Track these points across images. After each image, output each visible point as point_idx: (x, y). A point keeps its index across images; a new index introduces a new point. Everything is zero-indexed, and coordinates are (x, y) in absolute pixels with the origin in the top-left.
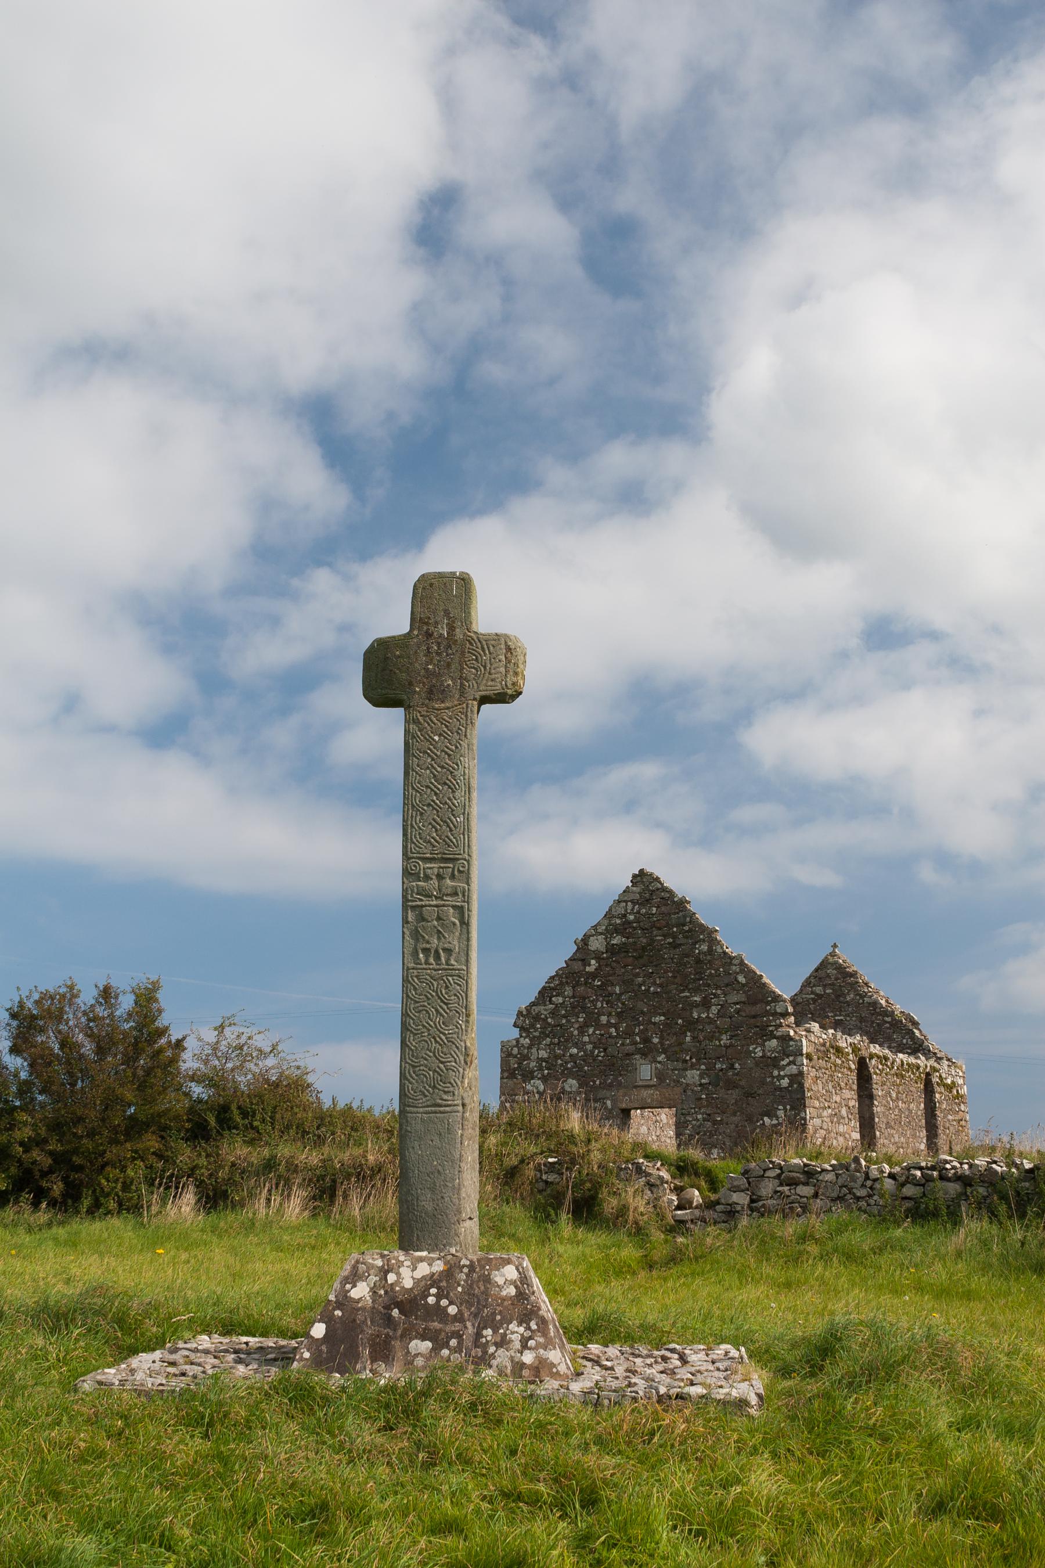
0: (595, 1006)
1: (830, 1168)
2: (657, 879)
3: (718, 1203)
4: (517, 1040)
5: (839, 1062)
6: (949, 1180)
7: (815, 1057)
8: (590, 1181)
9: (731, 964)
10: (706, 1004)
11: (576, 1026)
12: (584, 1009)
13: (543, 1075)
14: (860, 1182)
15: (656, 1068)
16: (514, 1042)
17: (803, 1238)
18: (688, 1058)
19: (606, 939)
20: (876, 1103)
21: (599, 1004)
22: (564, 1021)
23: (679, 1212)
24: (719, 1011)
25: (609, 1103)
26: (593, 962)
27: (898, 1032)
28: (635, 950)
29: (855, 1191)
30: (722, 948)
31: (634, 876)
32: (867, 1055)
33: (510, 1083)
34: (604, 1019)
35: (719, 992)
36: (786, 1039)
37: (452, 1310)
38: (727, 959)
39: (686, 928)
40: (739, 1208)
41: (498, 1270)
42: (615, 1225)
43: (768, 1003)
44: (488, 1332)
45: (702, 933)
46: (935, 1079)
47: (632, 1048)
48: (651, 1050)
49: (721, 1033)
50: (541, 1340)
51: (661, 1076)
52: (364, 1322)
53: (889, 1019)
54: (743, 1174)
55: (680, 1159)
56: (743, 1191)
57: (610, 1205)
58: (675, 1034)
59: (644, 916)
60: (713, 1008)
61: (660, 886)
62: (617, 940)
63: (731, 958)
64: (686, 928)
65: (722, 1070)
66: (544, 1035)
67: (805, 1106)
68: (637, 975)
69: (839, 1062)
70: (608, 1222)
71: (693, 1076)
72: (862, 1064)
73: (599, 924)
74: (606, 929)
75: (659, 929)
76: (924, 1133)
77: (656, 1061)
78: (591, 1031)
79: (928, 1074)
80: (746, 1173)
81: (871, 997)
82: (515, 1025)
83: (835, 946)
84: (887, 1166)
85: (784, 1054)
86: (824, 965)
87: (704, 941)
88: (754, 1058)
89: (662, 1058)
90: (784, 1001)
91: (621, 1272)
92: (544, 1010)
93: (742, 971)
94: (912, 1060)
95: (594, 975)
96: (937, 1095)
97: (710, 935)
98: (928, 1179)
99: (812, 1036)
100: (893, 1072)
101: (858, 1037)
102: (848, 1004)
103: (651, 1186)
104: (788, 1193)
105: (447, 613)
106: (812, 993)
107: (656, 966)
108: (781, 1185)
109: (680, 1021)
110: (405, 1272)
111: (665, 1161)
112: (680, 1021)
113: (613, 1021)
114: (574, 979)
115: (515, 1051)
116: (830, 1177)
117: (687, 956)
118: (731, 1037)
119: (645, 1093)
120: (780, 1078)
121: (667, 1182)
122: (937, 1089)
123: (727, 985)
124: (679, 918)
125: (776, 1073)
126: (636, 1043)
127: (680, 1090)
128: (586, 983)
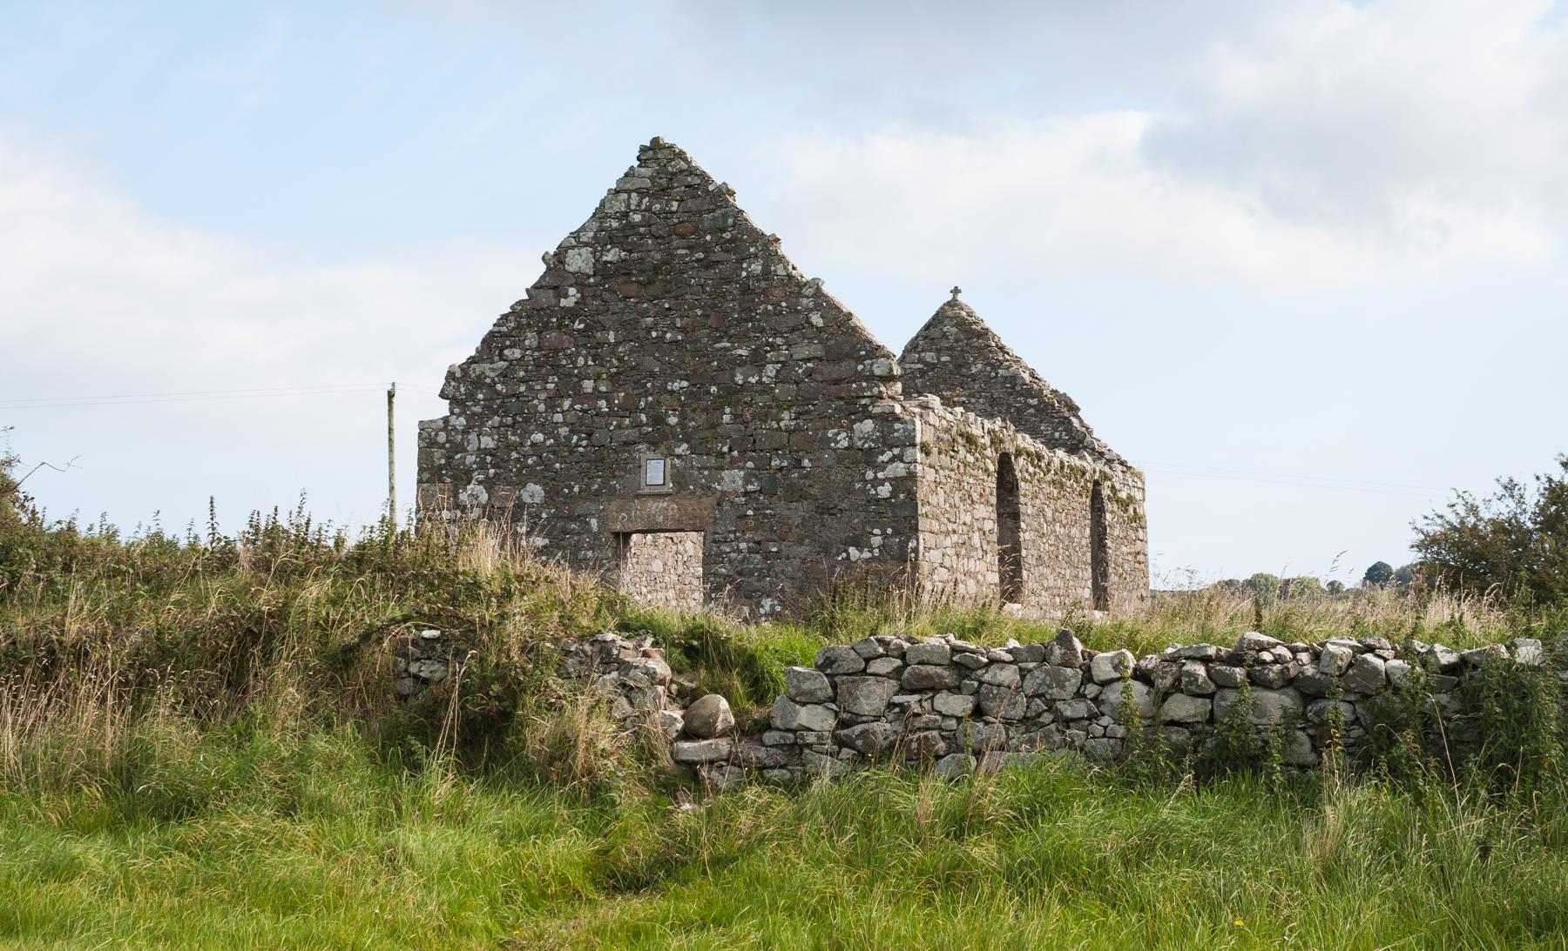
1: (1009, 657)
2: (681, 155)
3: (766, 725)
4: (446, 420)
5: (970, 459)
6: (1268, 685)
7: (935, 450)
8: (502, 679)
9: (800, 295)
11: (543, 396)
12: (556, 368)
13: (487, 477)
14: (1071, 688)
15: (673, 466)
16: (441, 424)
17: (962, 823)
18: (725, 449)
19: (594, 253)
20: (1023, 525)
21: (581, 361)
22: (522, 389)
23: (686, 745)
25: (594, 522)
26: (572, 291)
27: (1053, 419)
28: (642, 272)
29: (1060, 705)
30: (785, 268)
31: (643, 149)
32: (1012, 450)
34: (588, 385)
35: (779, 341)
36: (889, 418)
38: (795, 286)
39: (727, 235)
42: (545, 779)
43: (860, 360)
45: (753, 243)
46: (1106, 492)
47: (632, 434)
48: (664, 437)
49: (781, 409)
51: (680, 479)
53: (1034, 402)
54: (820, 668)
55: (696, 632)
57: (540, 730)
58: (705, 410)
60: (769, 367)
61: (685, 166)
62: (612, 255)
63: (801, 285)
64: (727, 235)
66: (490, 411)
67: (917, 530)
68: (644, 313)
69: (970, 459)
70: (530, 774)
71: (733, 479)
72: (1005, 463)
73: (583, 228)
74: (595, 237)
75: (683, 237)
76: (1088, 574)
77: (673, 455)
78: (567, 404)
79: (1097, 483)
80: (827, 664)
81: (1008, 368)
82: (443, 395)
83: (956, 291)
84: (1129, 655)
85: (884, 444)
86: (938, 320)
87: (756, 256)
88: (835, 450)
89: (682, 449)
90: (888, 356)
91: (543, 895)
94: (1075, 461)
95: (572, 313)
96: (1108, 516)
97: (767, 246)
98: (1224, 684)
99: (931, 418)
100: (1049, 477)
101: (999, 422)
102: (974, 378)
103: (627, 690)
104: (917, 710)
106: (920, 361)
108: (902, 690)
109: (713, 389)
111: (662, 637)
112: (713, 389)
113: (603, 389)
114: (541, 318)
115: (442, 437)
116: (1008, 675)
117: (728, 282)
118: (799, 415)
119: (654, 506)
120: (877, 482)
121: (662, 682)
122: (1108, 506)
124: (714, 219)
125: (870, 475)
126: (640, 425)
127: (709, 501)
128: (560, 326)
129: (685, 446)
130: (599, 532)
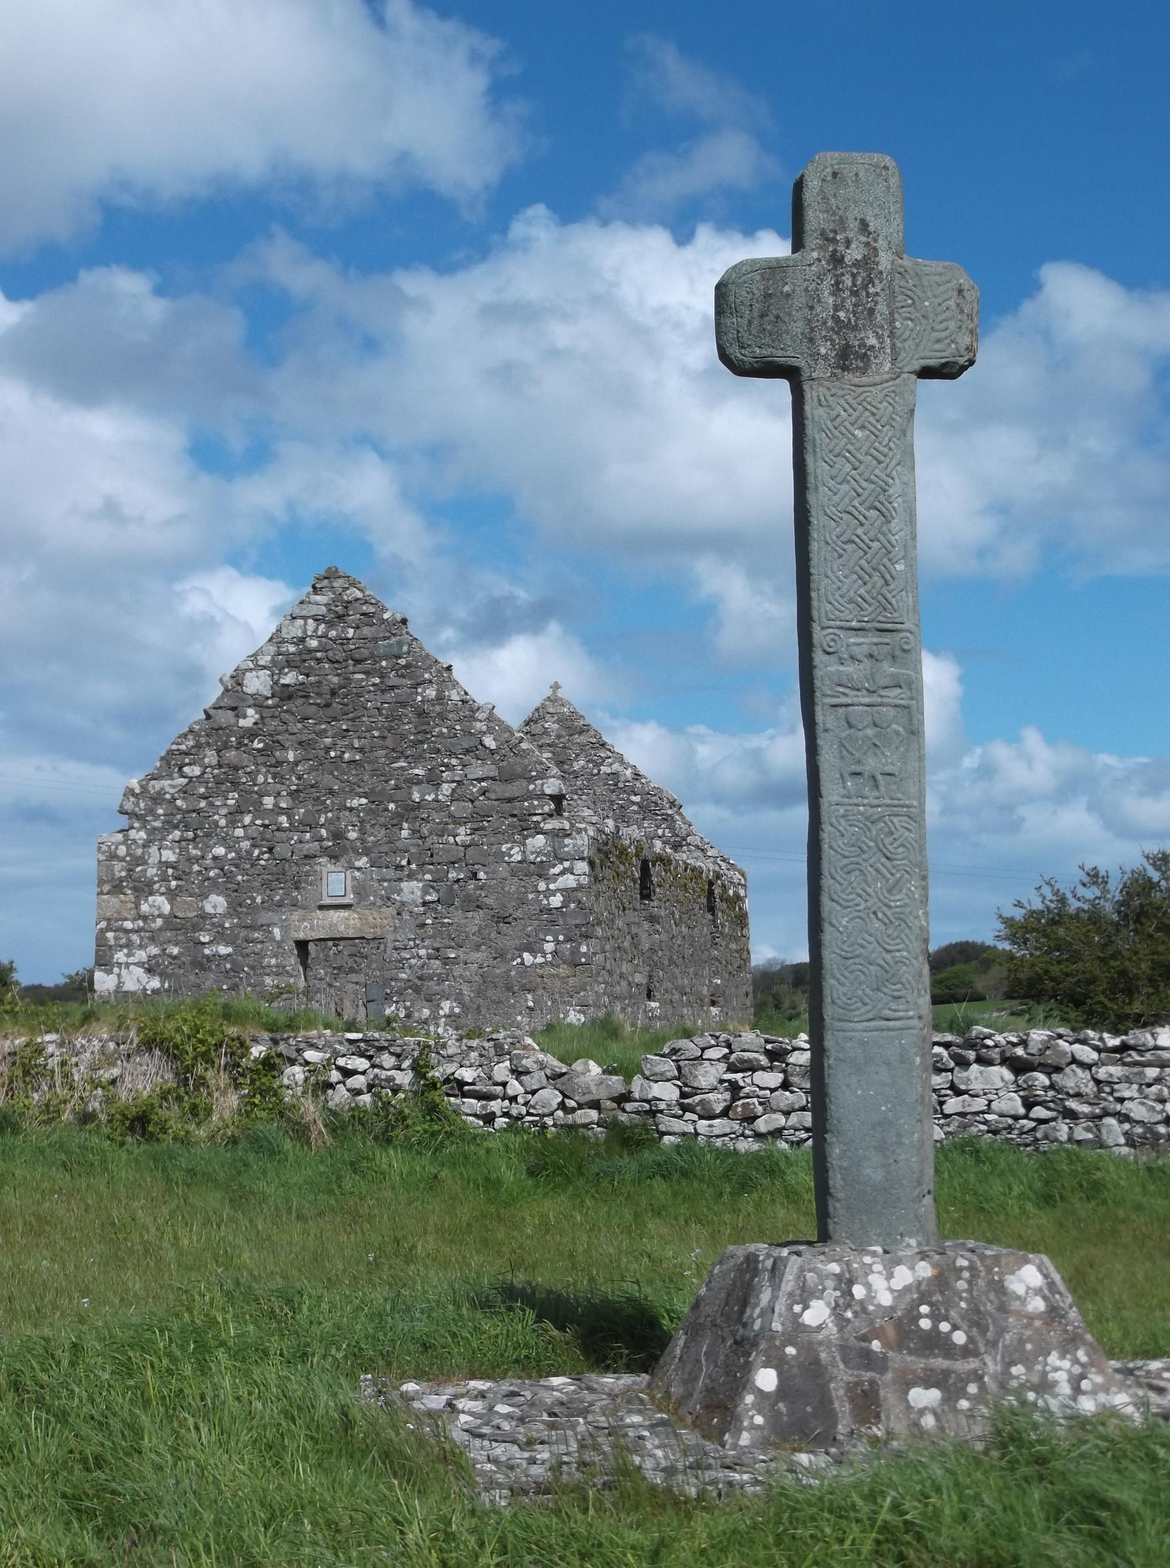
0: (254, 780)
10: (433, 780)
11: (224, 811)
12: (235, 784)
15: (354, 878)
18: (404, 863)
21: (261, 779)
24: (453, 790)
25: (277, 932)
26: (250, 712)
28: (319, 694)
33: (114, 901)
34: (269, 802)
35: (454, 761)
37: (959, 1338)
39: (402, 662)
40: (662, 1106)
41: (1013, 1273)
43: (531, 780)
44: (1018, 1370)
48: (345, 850)
50: (1099, 1379)
51: (361, 891)
52: (833, 1362)
56: (668, 1080)
59: (334, 640)
60: (445, 786)
61: (359, 595)
62: (289, 678)
64: (402, 662)
65: (458, 881)
66: (170, 825)
71: (412, 890)
78: (247, 819)
85: (556, 857)
87: (430, 682)
88: (509, 863)
89: (362, 862)
92: (169, 785)
93: (490, 731)
95: (252, 734)
105: (864, 225)
107: (353, 720)
109: (392, 806)
110: (877, 1281)
112: (392, 806)
113: (283, 805)
117: (403, 704)
120: (549, 893)
123: (467, 751)
124: (390, 646)
127: (392, 911)
128: (240, 744)
129: (365, 859)
130: (282, 941)
